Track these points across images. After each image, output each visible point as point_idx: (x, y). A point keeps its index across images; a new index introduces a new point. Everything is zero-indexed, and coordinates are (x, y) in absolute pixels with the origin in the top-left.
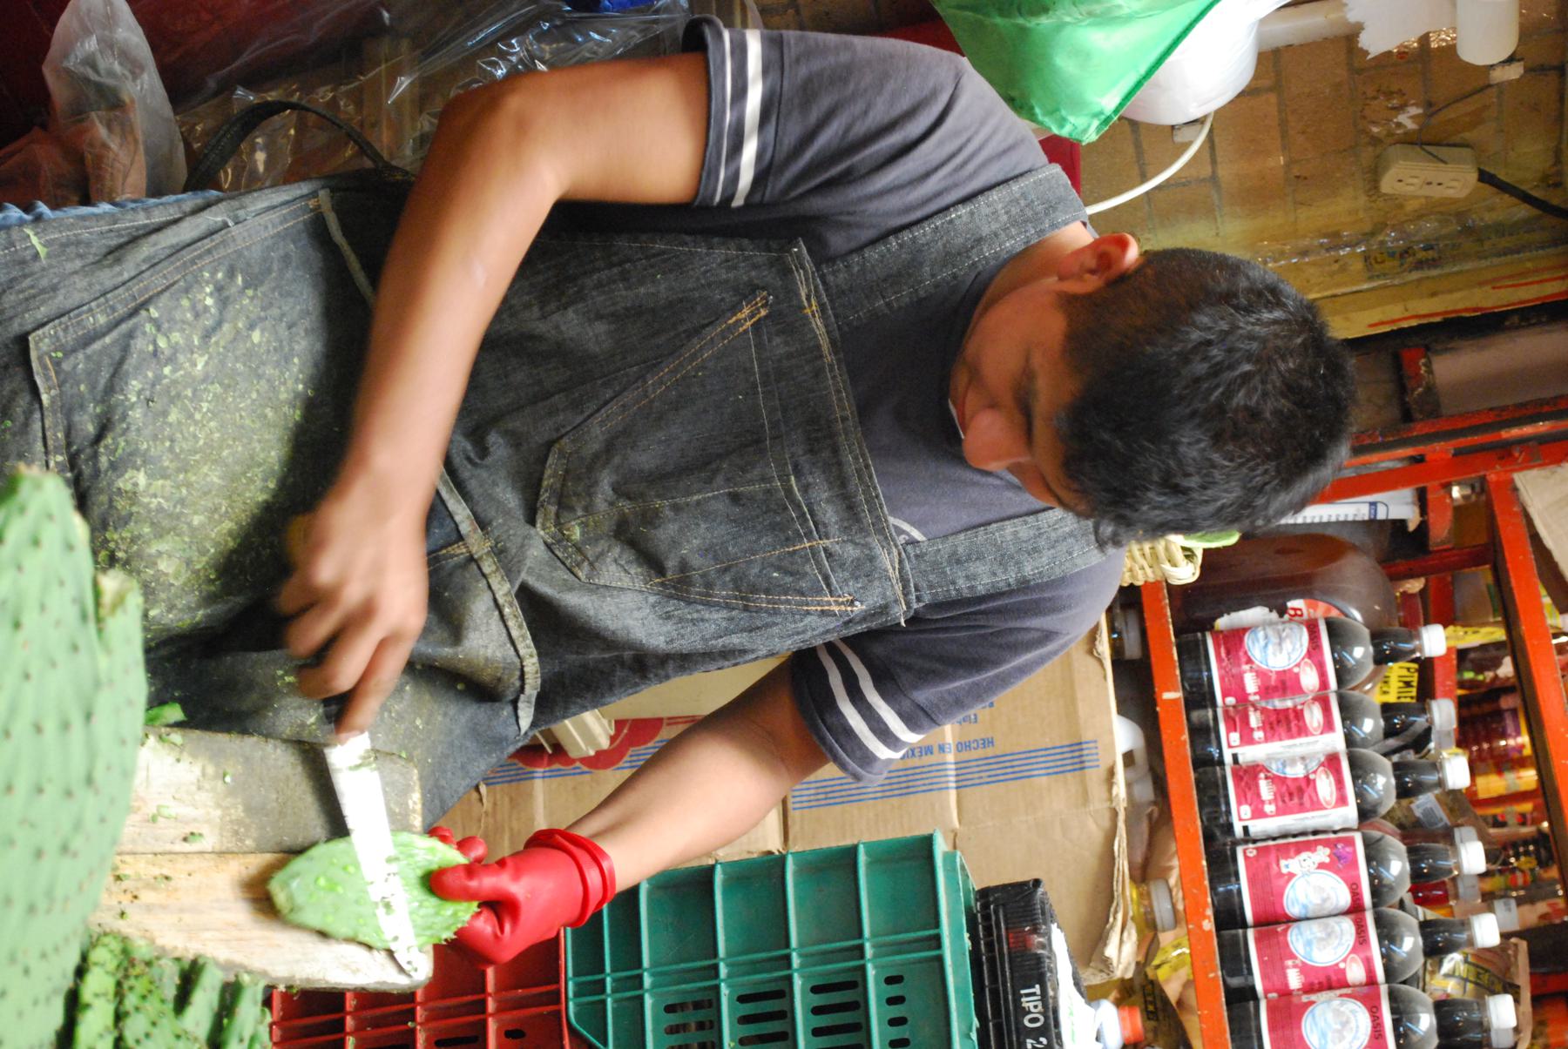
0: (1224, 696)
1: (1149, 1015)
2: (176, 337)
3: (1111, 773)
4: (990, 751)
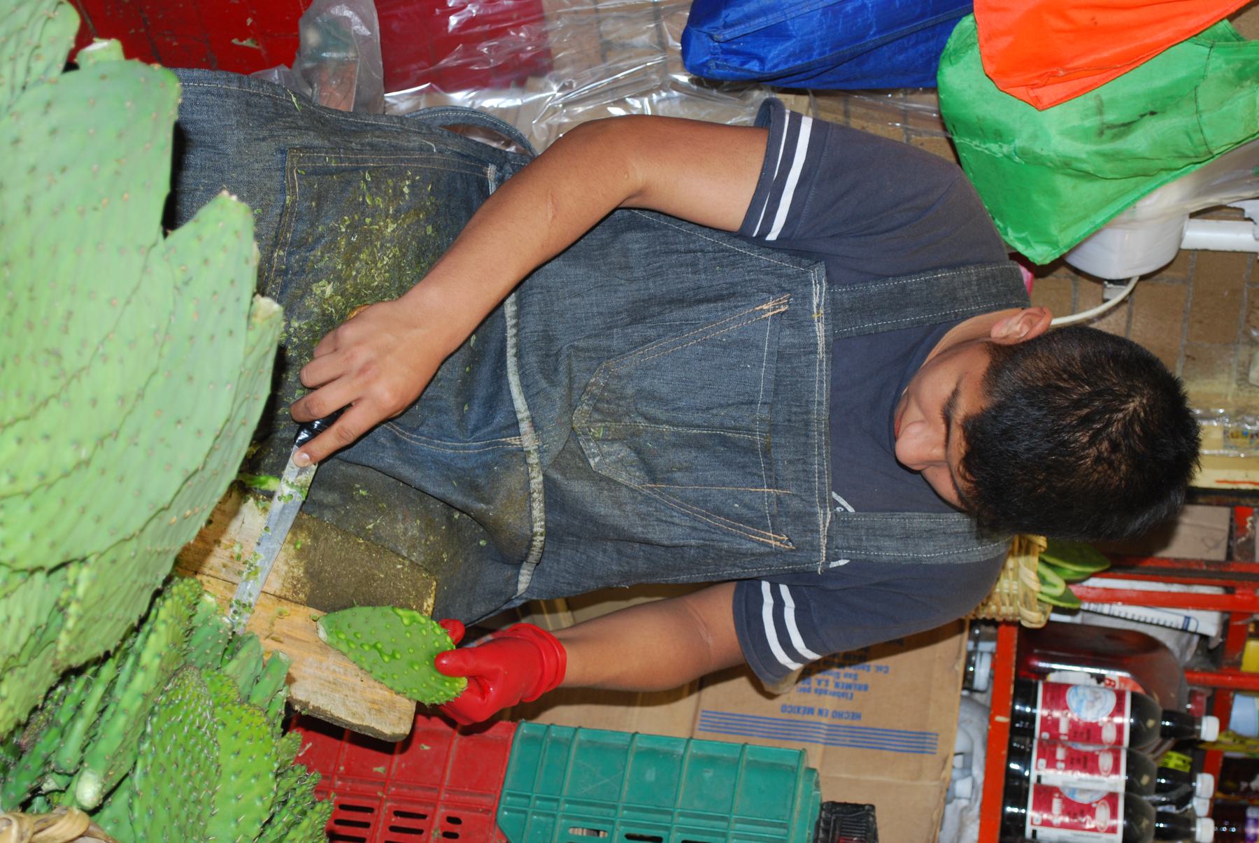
0: (1041, 731)
4: (856, 723)
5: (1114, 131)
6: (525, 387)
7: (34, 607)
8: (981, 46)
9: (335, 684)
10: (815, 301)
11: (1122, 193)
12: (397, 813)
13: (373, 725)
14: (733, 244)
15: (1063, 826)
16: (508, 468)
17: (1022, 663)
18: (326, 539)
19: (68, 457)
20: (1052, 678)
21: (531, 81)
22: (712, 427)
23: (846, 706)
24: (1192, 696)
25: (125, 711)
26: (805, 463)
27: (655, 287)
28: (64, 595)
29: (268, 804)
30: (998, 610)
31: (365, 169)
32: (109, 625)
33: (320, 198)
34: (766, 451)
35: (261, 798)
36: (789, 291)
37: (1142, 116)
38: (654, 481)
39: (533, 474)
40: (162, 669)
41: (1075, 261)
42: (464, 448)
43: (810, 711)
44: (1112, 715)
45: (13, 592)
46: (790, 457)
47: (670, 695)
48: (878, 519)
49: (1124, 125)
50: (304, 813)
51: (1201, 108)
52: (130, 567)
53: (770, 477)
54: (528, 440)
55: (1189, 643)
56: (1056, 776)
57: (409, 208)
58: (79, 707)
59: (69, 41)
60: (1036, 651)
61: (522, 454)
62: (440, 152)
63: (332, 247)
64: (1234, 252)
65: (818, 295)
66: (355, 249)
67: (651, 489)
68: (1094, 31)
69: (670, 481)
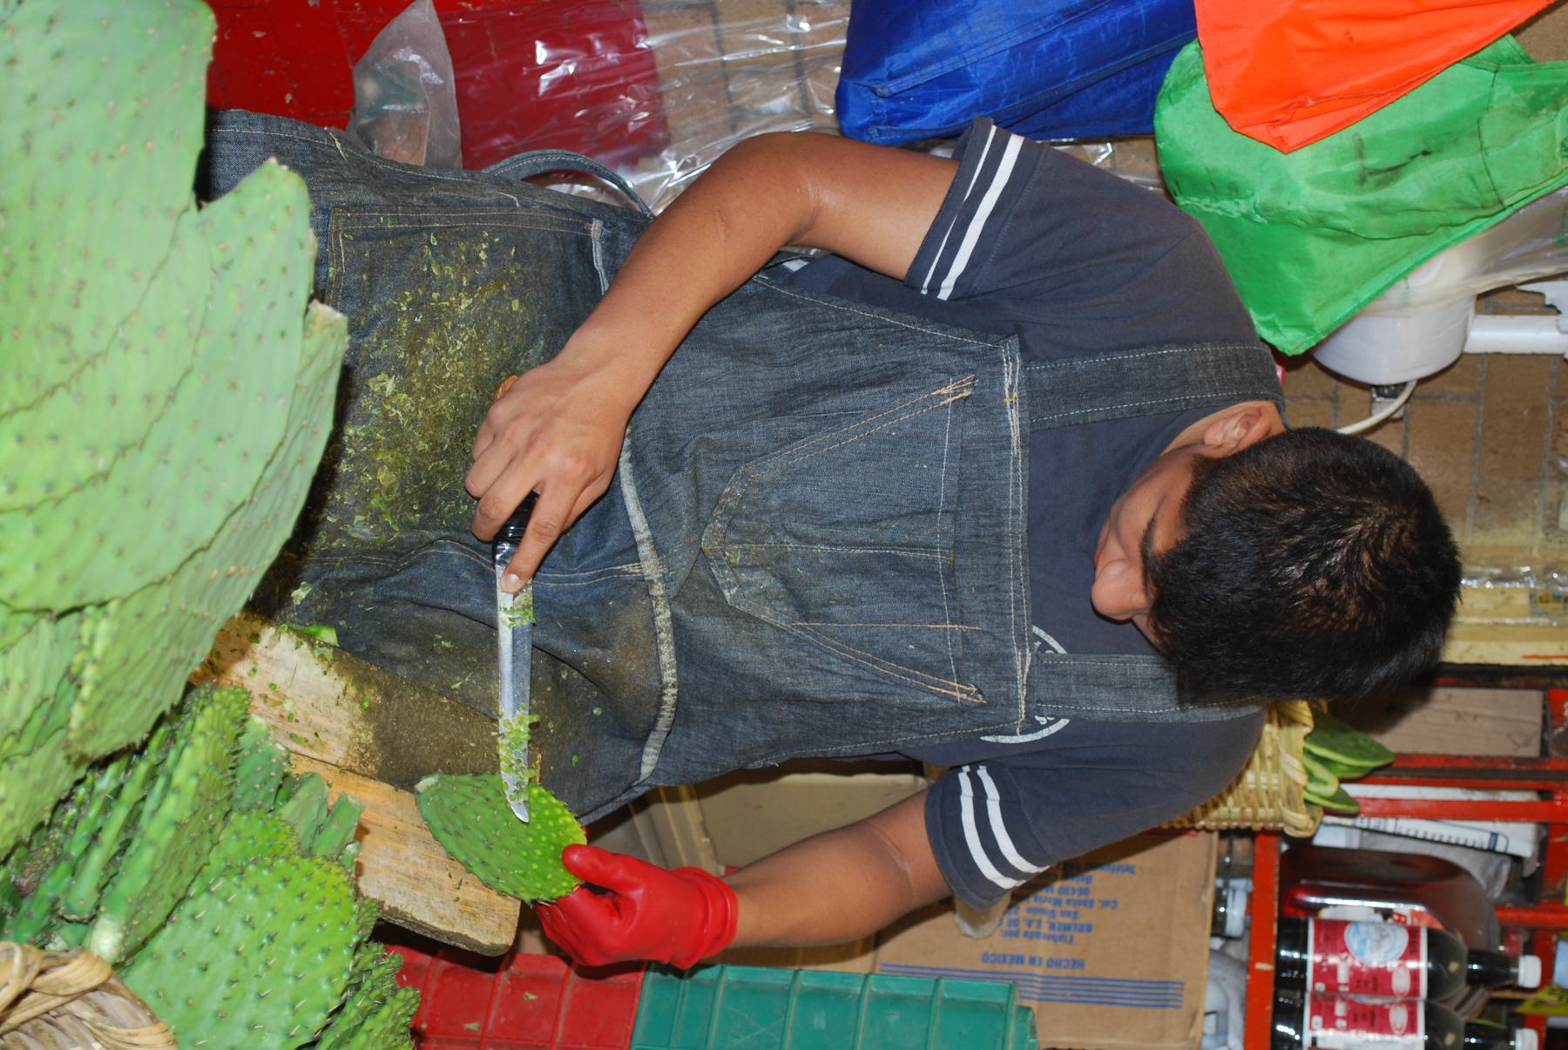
4: (1078, 973)
5: (1378, 177)
6: (646, 502)
8: (1208, 77)
9: (417, 880)
10: (1008, 381)
11: (1393, 261)
13: (466, 932)
14: (899, 319)
16: (626, 603)
17: (1287, 898)
18: (400, 697)
19: (81, 466)
20: (1325, 914)
21: (643, 162)
22: (881, 545)
23: (1065, 952)
24: (1504, 936)
25: (152, 843)
26: (997, 590)
27: (801, 374)
28: (78, 659)
29: (340, 988)
30: (1255, 814)
31: (429, 230)
32: (135, 705)
33: (373, 269)
34: (951, 572)
35: (330, 980)
36: (972, 371)
37: (1413, 157)
38: (806, 617)
39: (659, 609)
40: (199, 793)
41: (1332, 358)
42: (569, 580)
43: (1019, 959)
44: (1404, 957)
45: (12, 645)
46: (980, 583)
47: (842, 950)
48: (1091, 663)
49: (1390, 169)
50: (384, 1001)
51: (1487, 143)
52: (160, 630)
53: (954, 609)
57: (489, 278)
58: (94, 838)
60: (1303, 882)
61: (644, 585)
62: (525, 206)
63: (390, 331)
64: (1534, 354)
65: (1010, 376)
66: (419, 332)
67: (803, 628)
68: (1349, 49)
69: (827, 618)
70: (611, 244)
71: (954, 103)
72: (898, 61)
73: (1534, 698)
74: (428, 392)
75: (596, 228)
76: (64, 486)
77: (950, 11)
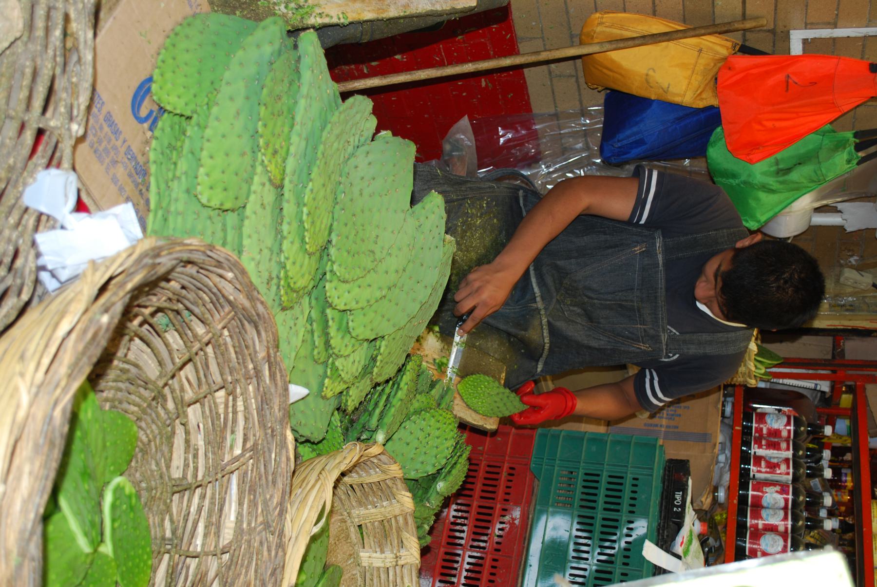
1: (710, 527)
2: (474, 211)
3: (715, 445)
6: (539, 284)
7: (363, 358)
10: (658, 245)
12: (489, 466)
15: (766, 472)
19: (378, 294)
21: (533, 165)
28: (375, 353)
43: (657, 425)
44: (786, 425)
48: (687, 336)
54: (540, 304)
55: (816, 396)
56: (761, 452)
58: (376, 404)
59: (373, 130)
61: (538, 310)
70: (525, 198)
71: (639, 149)
72: (621, 136)
73: (830, 339)
74: (467, 251)
75: (521, 193)
76: (373, 301)
77: (638, 119)
